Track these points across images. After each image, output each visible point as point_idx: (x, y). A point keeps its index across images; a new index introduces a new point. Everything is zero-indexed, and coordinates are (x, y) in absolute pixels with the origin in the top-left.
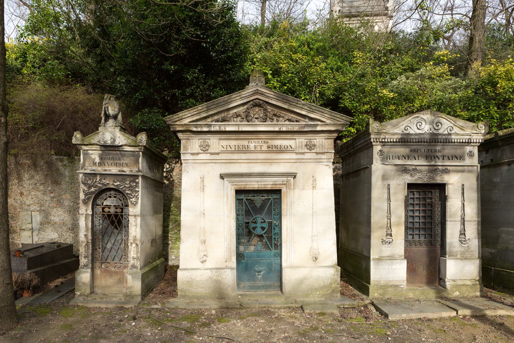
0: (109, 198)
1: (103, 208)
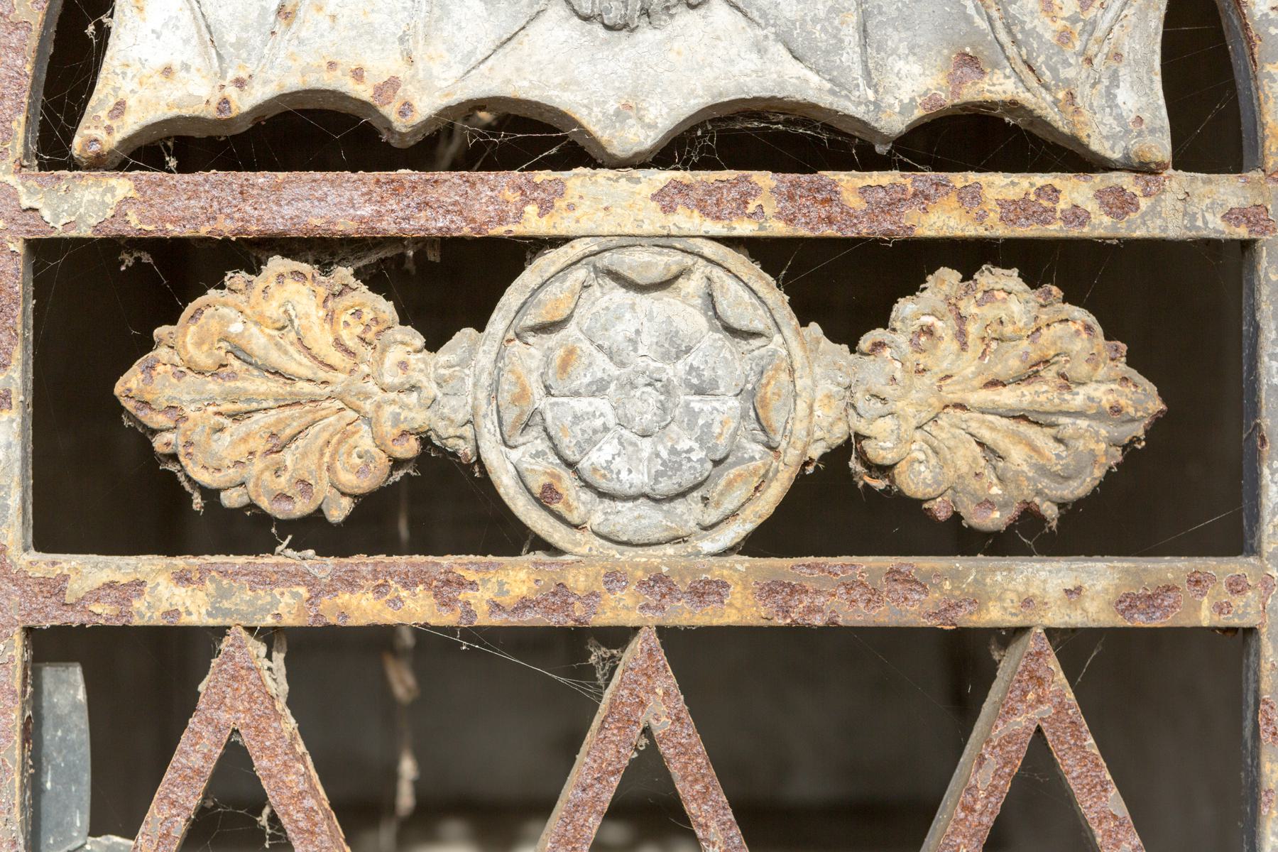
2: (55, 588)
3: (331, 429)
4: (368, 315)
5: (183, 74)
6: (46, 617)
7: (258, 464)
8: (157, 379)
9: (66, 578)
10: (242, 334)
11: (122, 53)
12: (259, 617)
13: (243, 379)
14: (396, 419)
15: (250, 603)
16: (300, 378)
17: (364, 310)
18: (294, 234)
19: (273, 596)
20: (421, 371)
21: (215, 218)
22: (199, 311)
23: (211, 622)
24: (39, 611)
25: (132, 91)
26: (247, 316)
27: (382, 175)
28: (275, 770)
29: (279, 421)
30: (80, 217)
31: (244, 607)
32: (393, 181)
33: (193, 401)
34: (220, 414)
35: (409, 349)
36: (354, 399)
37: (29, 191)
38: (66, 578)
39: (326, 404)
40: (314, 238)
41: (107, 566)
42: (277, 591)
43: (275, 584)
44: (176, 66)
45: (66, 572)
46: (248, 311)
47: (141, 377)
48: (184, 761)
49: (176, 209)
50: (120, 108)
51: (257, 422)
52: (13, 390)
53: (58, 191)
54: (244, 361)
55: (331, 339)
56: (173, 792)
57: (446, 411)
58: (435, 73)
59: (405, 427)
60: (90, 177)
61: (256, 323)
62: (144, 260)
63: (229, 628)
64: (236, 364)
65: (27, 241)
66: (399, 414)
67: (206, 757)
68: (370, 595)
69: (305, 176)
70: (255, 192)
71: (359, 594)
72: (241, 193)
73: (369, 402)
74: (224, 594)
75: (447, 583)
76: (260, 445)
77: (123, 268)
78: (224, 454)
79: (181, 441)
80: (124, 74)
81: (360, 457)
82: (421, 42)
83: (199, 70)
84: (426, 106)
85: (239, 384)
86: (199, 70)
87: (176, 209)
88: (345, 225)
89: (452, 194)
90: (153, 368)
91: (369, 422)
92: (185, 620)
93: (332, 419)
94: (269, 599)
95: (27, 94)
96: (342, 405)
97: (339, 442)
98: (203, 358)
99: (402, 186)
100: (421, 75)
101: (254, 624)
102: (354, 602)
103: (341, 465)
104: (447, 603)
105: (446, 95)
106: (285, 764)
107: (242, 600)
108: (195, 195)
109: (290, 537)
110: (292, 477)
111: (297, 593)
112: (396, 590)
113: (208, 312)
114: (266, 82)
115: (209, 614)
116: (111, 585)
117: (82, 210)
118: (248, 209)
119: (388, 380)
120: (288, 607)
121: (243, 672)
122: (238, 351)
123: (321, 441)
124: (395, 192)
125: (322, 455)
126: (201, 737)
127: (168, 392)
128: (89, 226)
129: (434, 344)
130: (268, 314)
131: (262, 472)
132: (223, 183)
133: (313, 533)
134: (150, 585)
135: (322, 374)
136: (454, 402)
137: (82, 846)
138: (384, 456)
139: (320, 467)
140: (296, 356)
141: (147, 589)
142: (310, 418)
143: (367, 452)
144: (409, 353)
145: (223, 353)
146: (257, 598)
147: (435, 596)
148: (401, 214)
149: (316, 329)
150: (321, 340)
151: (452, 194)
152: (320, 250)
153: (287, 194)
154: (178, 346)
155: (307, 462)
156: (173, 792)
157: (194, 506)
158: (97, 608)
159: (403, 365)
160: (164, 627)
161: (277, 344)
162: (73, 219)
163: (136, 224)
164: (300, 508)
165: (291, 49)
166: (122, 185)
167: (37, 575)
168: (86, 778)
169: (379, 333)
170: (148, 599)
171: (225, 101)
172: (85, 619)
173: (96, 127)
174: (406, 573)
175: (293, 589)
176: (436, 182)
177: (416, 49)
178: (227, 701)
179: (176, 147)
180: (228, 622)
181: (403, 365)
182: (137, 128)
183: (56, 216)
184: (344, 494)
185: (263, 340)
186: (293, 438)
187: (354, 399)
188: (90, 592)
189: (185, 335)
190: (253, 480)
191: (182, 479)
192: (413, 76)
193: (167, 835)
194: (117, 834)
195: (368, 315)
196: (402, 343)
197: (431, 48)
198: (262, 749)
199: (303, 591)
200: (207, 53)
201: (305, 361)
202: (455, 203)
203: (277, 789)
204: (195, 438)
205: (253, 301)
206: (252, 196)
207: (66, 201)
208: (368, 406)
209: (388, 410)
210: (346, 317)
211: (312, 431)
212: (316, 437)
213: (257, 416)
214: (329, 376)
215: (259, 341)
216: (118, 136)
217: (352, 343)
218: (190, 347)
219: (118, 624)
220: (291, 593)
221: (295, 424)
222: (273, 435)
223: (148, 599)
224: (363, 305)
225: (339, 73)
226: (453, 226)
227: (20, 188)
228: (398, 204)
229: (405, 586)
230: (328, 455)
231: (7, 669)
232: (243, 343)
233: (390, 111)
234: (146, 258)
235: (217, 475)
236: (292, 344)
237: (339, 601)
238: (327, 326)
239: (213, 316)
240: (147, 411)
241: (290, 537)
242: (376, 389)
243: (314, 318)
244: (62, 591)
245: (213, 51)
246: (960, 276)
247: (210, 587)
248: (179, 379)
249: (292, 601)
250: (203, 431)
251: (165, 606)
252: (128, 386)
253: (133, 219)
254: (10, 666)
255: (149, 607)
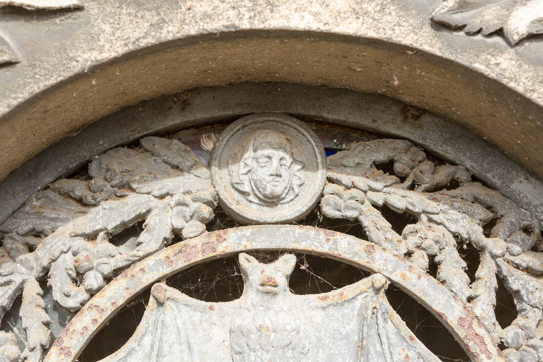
0: (177, 316)
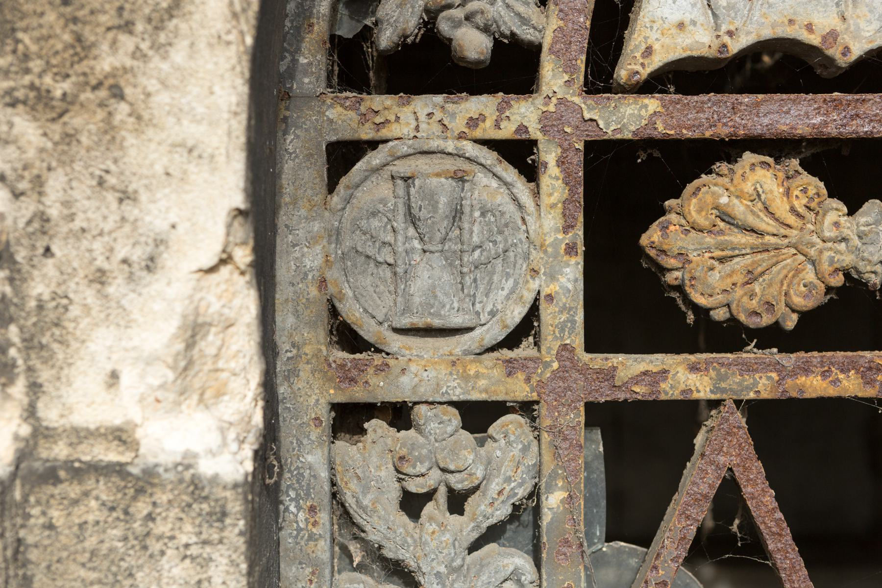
1: (626, 189)
2: (609, 375)
3: (789, 267)
4: (812, 191)
5: (691, 27)
6: (602, 395)
7: (739, 292)
8: (671, 235)
9: (615, 368)
10: (728, 204)
11: (651, 13)
12: (744, 393)
13: (729, 234)
14: (832, 261)
15: (739, 384)
16: (768, 234)
17: (810, 188)
18: (768, 136)
19: (754, 379)
20: (849, 228)
21: (715, 126)
22: (698, 189)
23: (713, 397)
24: (597, 391)
25: (657, 39)
26: (731, 193)
27: (827, 96)
28: (756, 494)
29: (754, 263)
30: (624, 125)
31: (735, 387)
32: (835, 100)
33: (695, 250)
34: (713, 258)
35: (840, 214)
36: (804, 247)
37: (588, 108)
38: (615, 368)
39: (785, 251)
40: (781, 139)
41: (643, 360)
42: (757, 376)
43: (756, 371)
44: (687, 21)
45: (615, 365)
46: (732, 189)
47: (659, 233)
48: (695, 489)
49: (689, 120)
50: (649, 51)
51: (737, 263)
52: (579, 242)
53: (608, 107)
54: (728, 223)
55: (788, 208)
56: (687, 510)
57: (865, 254)
58: (861, 27)
59: (837, 265)
60: (631, 98)
61: (737, 197)
62: (655, 155)
63: (724, 400)
64: (722, 225)
65: (586, 141)
66: (834, 257)
67: (711, 486)
68: (819, 378)
69: (778, 96)
70: (743, 108)
71: (811, 377)
72: (733, 108)
73: (814, 249)
74: (722, 378)
75: (870, 369)
76: (739, 278)
77: (639, 161)
78: (716, 285)
79: (687, 276)
80: (652, 27)
81: (805, 286)
82: (851, 6)
83: (702, 25)
84: (858, 50)
85: (726, 238)
86: (702, 25)
87: (689, 120)
88: (803, 129)
89: (874, 108)
90: (667, 228)
91: (813, 263)
92: (696, 396)
93: (788, 261)
94: (752, 381)
95: (587, 41)
96: (795, 252)
97: (794, 276)
98: (702, 220)
99: (841, 103)
100: (852, 28)
101: (742, 397)
102: (809, 382)
103: (796, 289)
104: (870, 382)
105: (871, 42)
106: (763, 490)
107: (734, 381)
108: (701, 110)
109: (755, 341)
110: (760, 300)
111: (771, 377)
112: (836, 374)
113: (704, 189)
114: (748, 33)
115: (712, 392)
116: (645, 373)
117: (625, 121)
118: (737, 119)
119: (827, 234)
120: (763, 386)
121: (735, 430)
122: (725, 216)
123: (781, 276)
124: (836, 108)
125: (782, 284)
126: (707, 474)
127: (680, 244)
128: (630, 131)
129: (851, 212)
130: (746, 190)
131: (742, 297)
132: (720, 101)
133: (772, 337)
134: (672, 372)
135: (783, 231)
136: (871, 249)
137: (601, 549)
138: (823, 285)
139: (780, 293)
140: (765, 218)
141: (670, 376)
142: (774, 260)
143: (811, 283)
144: (840, 216)
145: (713, 217)
146: (744, 380)
147: (862, 378)
148: (840, 122)
149: (778, 201)
150: (781, 207)
151: (874, 108)
152: (776, 147)
153: (763, 109)
154: (686, 213)
155: (772, 290)
156: (687, 510)
157: (688, 321)
158: (637, 389)
159: (837, 224)
160: (681, 401)
161: (752, 211)
162: (619, 126)
163: (661, 129)
164: (766, 320)
165: (764, 10)
166: (652, 103)
167: (596, 367)
168: (604, 503)
169: (819, 203)
170: (671, 382)
171: (724, 46)
172: (628, 396)
173: (635, 64)
174: (843, 363)
175: (762, 376)
176: (864, 100)
177: (847, 10)
178: (725, 449)
179: (686, 77)
180: (724, 396)
181: (837, 224)
182: (661, 64)
183: (608, 125)
184: (794, 311)
185: (742, 208)
186: (762, 273)
187: (804, 247)
188: (632, 378)
189: (689, 205)
190: (735, 302)
191: (680, 302)
192: (846, 29)
193: (685, 538)
194: (622, 541)
195: (812, 191)
196: (837, 209)
197: (858, 10)
198: (748, 480)
199: (774, 375)
200: (707, 13)
201: (771, 222)
202: (876, 115)
203: (757, 506)
204: (697, 274)
205: (735, 181)
206: (740, 111)
207: (614, 115)
208: (812, 252)
209: (827, 254)
210: (797, 192)
211: (775, 269)
212: (779, 273)
213: (736, 260)
214: (787, 232)
215: (739, 209)
216: (649, 70)
217: (801, 210)
218: (693, 213)
219: (650, 399)
220: (767, 376)
221: (764, 264)
222: (749, 272)
223: (671, 382)
224: (809, 184)
225: (797, 27)
226: (875, 130)
227: (583, 106)
228: (838, 115)
229: (842, 371)
230: (785, 285)
231: (575, 430)
232: (729, 210)
233: (834, 52)
234: (657, 154)
235: (711, 299)
236: (761, 211)
237: (798, 382)
238: (785, 199)
239: (707, 192)
240: (664, 257)
241: (755, 341)
242: (818, 240)
243: (776, 193)
244: (613, 377)
245: (710, 12)
246: (242, 206)
247: (712, 373)
248: (686, 235)
249: (767, 382)
250: (702, 270)
251: (682, 387)
252: (652, 239)
253: (660, 127)
254: (577, 428)
255: (672, 387)
